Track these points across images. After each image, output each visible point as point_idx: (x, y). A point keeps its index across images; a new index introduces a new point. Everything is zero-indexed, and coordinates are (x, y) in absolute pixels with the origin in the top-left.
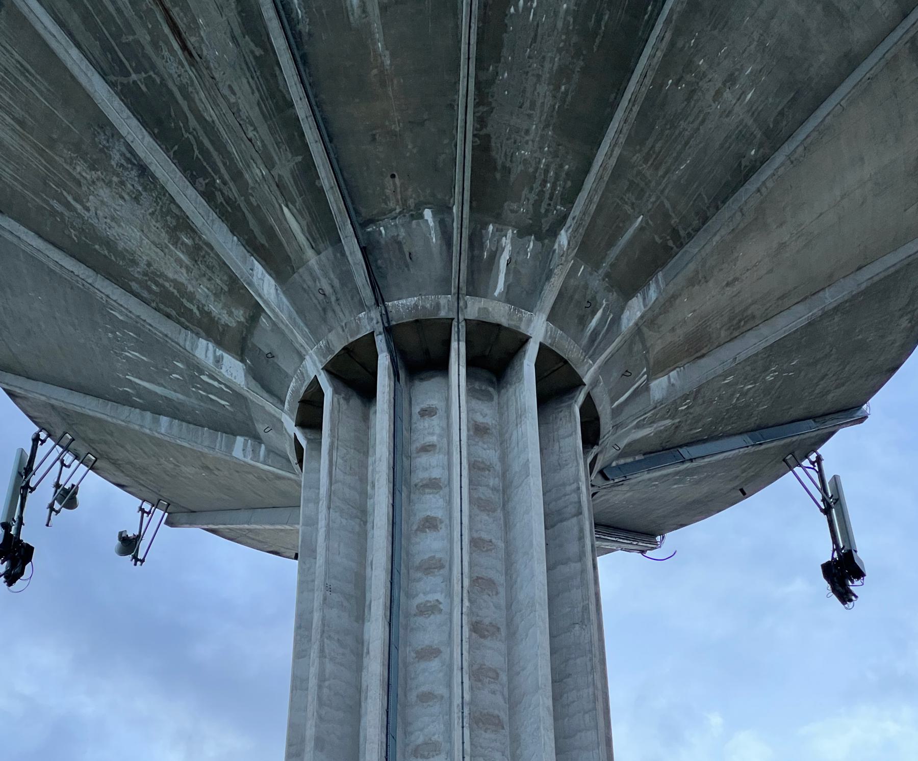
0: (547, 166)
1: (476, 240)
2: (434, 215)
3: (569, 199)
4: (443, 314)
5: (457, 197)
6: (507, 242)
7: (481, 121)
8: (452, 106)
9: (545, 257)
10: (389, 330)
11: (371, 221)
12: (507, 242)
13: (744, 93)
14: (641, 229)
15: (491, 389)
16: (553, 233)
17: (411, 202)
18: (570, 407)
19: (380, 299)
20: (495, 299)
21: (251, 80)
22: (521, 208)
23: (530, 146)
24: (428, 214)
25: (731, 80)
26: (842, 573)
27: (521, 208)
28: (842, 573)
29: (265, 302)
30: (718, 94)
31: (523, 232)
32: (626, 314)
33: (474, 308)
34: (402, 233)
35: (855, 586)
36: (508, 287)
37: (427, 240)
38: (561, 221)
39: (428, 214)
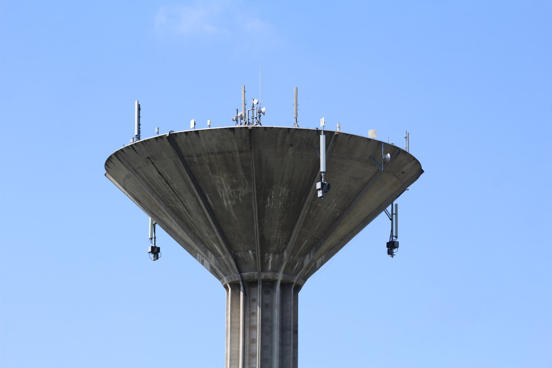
0: (280, 239)
1: (262, 258)
2: (252, 252)
3: (286, 243)
4: (256, 277)
5: (253, 200)
6: (271, 257)
7: (261, 231)
8: (253, 229)
9: (281, 258)
10: (242, 281)
11: (236, 252)
12: (271, 257)
13: (333, 205)
14: (307, 242)
15: (270, 289)
16: (283, 251)
17: (246, 249)
18: (291, 290)
19: (240, 272)
20: (269, 271)
21: (201, 236)
22: (274, 248)
23: (275, 234)
24: (250, 251)
25: (329, 204)
26: (392, 246)
27: (274, 248)
28: (392, 246)
29: (194, 196)
30: (325, 209)
31: (275, 254)
32: (305, 260)
33: (263, 276)
34: (244, 256)
35: (395, 250)
36: (272, 267)
37: (251, 258)
38: (285, 248)
39: (250, 251)
